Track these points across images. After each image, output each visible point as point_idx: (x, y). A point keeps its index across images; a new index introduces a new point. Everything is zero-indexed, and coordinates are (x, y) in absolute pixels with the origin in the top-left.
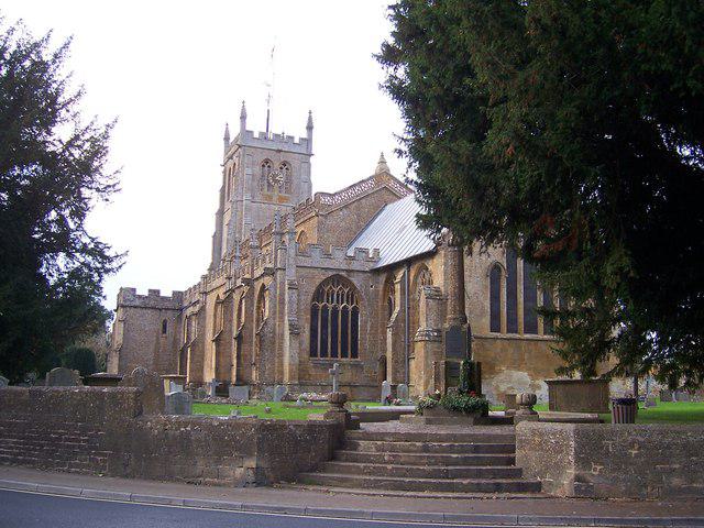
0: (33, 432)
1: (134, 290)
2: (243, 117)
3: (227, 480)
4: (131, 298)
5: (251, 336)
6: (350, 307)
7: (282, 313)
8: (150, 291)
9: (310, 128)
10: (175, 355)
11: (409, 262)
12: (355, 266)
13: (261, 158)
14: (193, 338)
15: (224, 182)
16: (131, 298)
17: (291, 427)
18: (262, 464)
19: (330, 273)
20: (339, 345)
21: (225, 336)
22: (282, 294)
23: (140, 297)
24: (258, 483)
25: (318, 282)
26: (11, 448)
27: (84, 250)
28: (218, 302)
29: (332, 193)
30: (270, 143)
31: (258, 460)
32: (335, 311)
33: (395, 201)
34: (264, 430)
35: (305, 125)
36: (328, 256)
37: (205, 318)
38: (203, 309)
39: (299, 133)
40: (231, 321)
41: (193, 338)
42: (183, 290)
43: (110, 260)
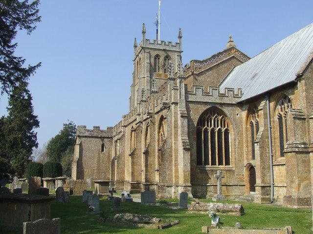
1: (85, 127)
2: (144, 33)
4: (83, 131)
6: (223, 130)
7: (176, 133)
9: (180, 37)
10: (109, 163)
11: (268, 95)
12: (226, 100)
13: (154, 53)
14: (118, 153)
16: (83, 131)
20: (217, 156)
21: (137, 152)
22: (176, 121)
23: (88, 131)
25: (201, 112)
28: (133, 130)
29: (202, 60)
30: (159, 45)
32: (220, 130)
33: (240, 64)
35: (178, 36)
36: (207, 94)
37: (124, 141)
38: (124, 135)
40: (140, 142)
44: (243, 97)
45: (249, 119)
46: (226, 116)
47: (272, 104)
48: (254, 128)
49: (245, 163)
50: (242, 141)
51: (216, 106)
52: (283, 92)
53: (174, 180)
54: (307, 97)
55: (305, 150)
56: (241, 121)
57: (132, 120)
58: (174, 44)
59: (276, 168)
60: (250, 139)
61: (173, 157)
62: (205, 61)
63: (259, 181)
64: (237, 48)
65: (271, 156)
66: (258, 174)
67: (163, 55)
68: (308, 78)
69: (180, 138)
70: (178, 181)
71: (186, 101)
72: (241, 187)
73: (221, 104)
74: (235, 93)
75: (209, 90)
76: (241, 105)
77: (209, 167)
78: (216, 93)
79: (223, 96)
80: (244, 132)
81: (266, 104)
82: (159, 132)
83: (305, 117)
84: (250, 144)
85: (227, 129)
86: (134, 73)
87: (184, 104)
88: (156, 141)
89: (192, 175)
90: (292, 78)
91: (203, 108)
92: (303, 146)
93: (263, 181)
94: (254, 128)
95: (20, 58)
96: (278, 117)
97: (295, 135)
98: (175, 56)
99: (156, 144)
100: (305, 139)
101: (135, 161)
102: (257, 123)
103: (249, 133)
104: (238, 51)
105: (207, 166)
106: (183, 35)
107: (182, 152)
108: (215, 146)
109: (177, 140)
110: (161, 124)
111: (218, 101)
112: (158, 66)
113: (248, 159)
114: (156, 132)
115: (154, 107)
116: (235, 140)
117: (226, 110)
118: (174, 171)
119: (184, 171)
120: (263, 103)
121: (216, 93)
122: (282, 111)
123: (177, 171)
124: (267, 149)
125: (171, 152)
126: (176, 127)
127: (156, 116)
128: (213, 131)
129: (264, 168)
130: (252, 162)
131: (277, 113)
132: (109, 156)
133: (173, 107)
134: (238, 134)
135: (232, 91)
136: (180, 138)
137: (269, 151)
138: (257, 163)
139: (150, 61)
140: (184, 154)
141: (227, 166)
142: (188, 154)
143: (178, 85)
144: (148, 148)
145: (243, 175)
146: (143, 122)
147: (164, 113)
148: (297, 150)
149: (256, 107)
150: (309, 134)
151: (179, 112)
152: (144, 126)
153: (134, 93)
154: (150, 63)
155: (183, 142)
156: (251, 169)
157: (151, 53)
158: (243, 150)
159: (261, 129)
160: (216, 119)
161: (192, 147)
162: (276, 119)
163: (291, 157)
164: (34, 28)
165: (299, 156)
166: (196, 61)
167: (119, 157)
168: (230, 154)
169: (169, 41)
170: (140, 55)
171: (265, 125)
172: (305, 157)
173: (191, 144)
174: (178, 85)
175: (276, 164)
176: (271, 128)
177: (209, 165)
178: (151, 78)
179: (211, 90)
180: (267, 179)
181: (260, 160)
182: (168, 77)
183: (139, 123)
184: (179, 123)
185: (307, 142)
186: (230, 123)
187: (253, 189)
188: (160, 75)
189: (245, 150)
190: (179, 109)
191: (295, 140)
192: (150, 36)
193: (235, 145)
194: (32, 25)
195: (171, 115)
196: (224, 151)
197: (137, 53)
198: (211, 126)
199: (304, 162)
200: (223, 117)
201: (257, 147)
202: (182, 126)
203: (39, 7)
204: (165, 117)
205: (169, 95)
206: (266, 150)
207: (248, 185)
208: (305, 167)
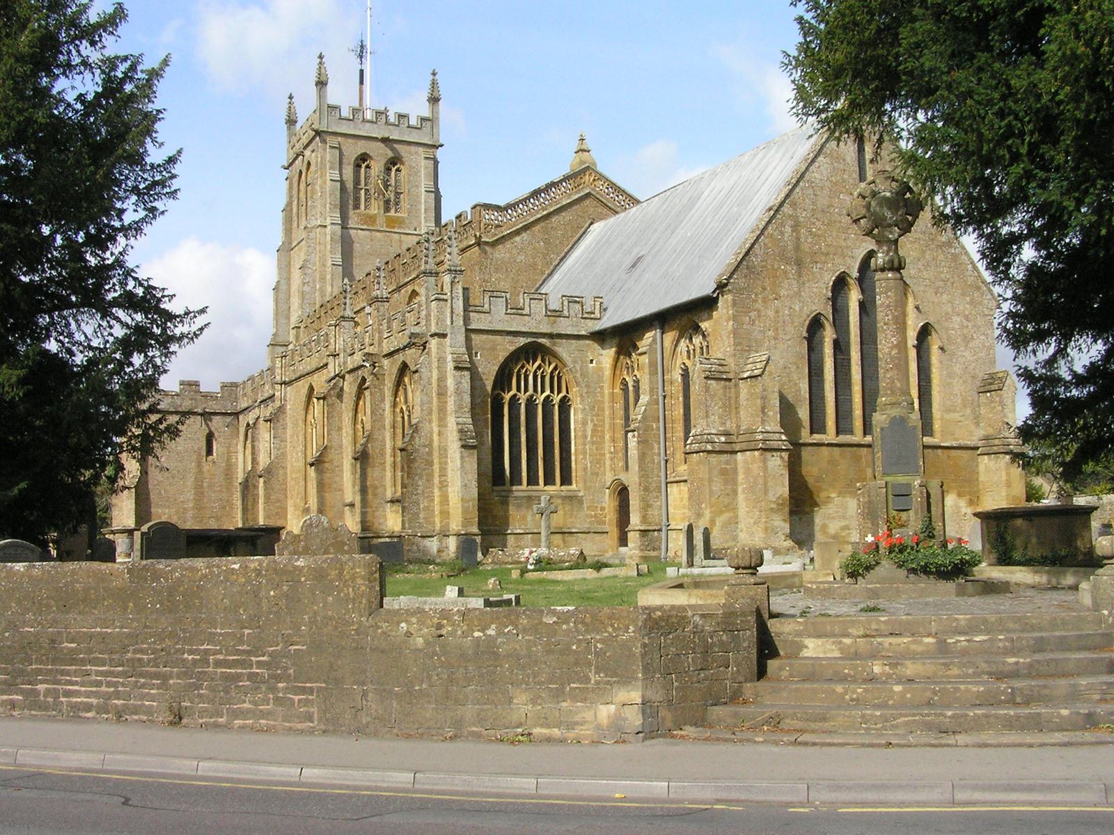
0: (142, 651)
2: (321, 84)
3: (578, 731)
5: (383, 454)
6: (557, 399)
7: (442, 410)
8: (182, 383)
9: (434, 100)
11: (662, 319)
12: (564, 327)
13: (353, 150)
15: (291, 197)
17: (697, 618)
18: (651, 694)
19: (522, 341)
21: (332, 455)
22: (442, 379)
24: (650, 732)
26: (99, 684)
27: (129, 302)
29: (502, 204)
31: (645, 688)
32: (547, 402)
34: (651, 629)
36: (517, 311)
38: (281, 409)
39: (418, 108)
40: (340, 429)
41: (263, 461)
42: (239, 380)
43: (170, 316)
44: (605, 319)
45: (618, 372)
46: (565, 365)
47: (670, 337)
48: (629, 394)
49: (609, 478)
50: (603, 426)
51: (541, 340)
52: (690, 316)
53: (437, 520)
54: (735, 332)
55: (727, 447)
56: (600, 378)
57: (309, 368)
58: (413, 121)
59: (673, 489)
60: (620, 422)
61: (436, 467)
62: (513, 206)
63: (635, 519)
64: (600, 169)
65: (663, 463)
66: (634, 503)
67: (380, 155)
68: (740, 290)
69: (451, 421)
70: (448, 524)
71: (467, 330)
72: (598, 537)
73: (551, 336)
74: (588, 308)
75: (522, 300)
76: (600, 337)
77: (522, 489)
78: (538, 308)
79: (557, 314)
80: (607, 405)
81: (654, 340)
82: (395, 405)
83: (731, 376)
84: (620, 434)
85: (565, 397)
86: (287, 210)
87: (461, 338)
88: (388, 426)
89: (480, 509)
90: (707, 289)
91: (508, 346)
92: (723, 439)
93: (644, 519)
94: (629, 394)
95: (163, 289)
96: (680, 372)
97: (707, 416)
98: (416, 160)
99: (388, 435)
100: (728, 423)
101: (326, 481)
102: (637, 382)
103: (619, 406)
104: (601, 177)
105: (514, 488)
106: (443, 92)
107: (458, 455)
108: (537, 437)
109: (446, 426)
110: (399, 382)
111: (544, 329)
112: (367, 190)
113: (613, 469)
114: (387, 405)
115: (381, 340)
116: (584, 423)
117: (564, 350)
118: (437, 500)
119: (463, 500)
120: (649, 336)
121: (538, 308)
122: (689, 358)
123: (445, 500)
124: (656, 446)
125: (430, 453)
126: (442, 393)
127: (386, 362)
128: (530, 403)
129: (646, 489)
130: (623, 477)
131: (679, 362)
132: (229, 472)
133: (433, 343)
134: (592, 409)
135: (578, 302)
136: (451, 421)
137: (659, 449)
138: (632, 479)
139: (341, 176)
140: (462, 457)
141: (563, 488)
142: (472, 464)
143: (447, 289)
144: (365, 445)
145: (603, 509)
146: (347, 376)
147: (410, 355)
148: (709, 447)
149: (636, 347)
150: (737, 413)
151: (449, 358)
152: (349, 386)
153: (289, 272)
154: (342, 182)
155: (461, 431)
156: (622, 493)
157: (344, 148)
158: (603, 448)
159: (644, 399)
160: (539, 373)
161: (481, 443)
162: (677, 376)
163: (699, 463)
164: (163, 213)
165: (714, 459)
166: (487, 207)
167: (269, 472)
168: (573, 458)
169: (403, 111)
170: (307, 153)
171: (652, 390)
172: (727, 463)
173: (479, 435)
174: (447, 289)
175: (675, 479)
176: (665, 397)
177: (521, 484)
178: (344, 227)
179: (527, 301)
180: (654, 513)
181: (639, 472)
182: (423, 268)
183: (333, 378)
184: (450, 383)
185: (734, 430)
186: (572, 383)
187: (623, 541)
188: (371, 219)
189: (608, 447)
190: (449, 350)
191: (708, 426)
192: (341, 94)
193: (585, 437)
194: (159, 205)
195: (430, 363)
196: (557, 451)
197: (299, 147)
198: (526, 390)
199: (724, 472)
200: (555, 368)
201: (633, 441)
202: (458, 391)
203: (177, 169)
204: (413, 368)
205: (423, 313)
206: (652, 448)
207: (614, 532)
208: (726, 483)
